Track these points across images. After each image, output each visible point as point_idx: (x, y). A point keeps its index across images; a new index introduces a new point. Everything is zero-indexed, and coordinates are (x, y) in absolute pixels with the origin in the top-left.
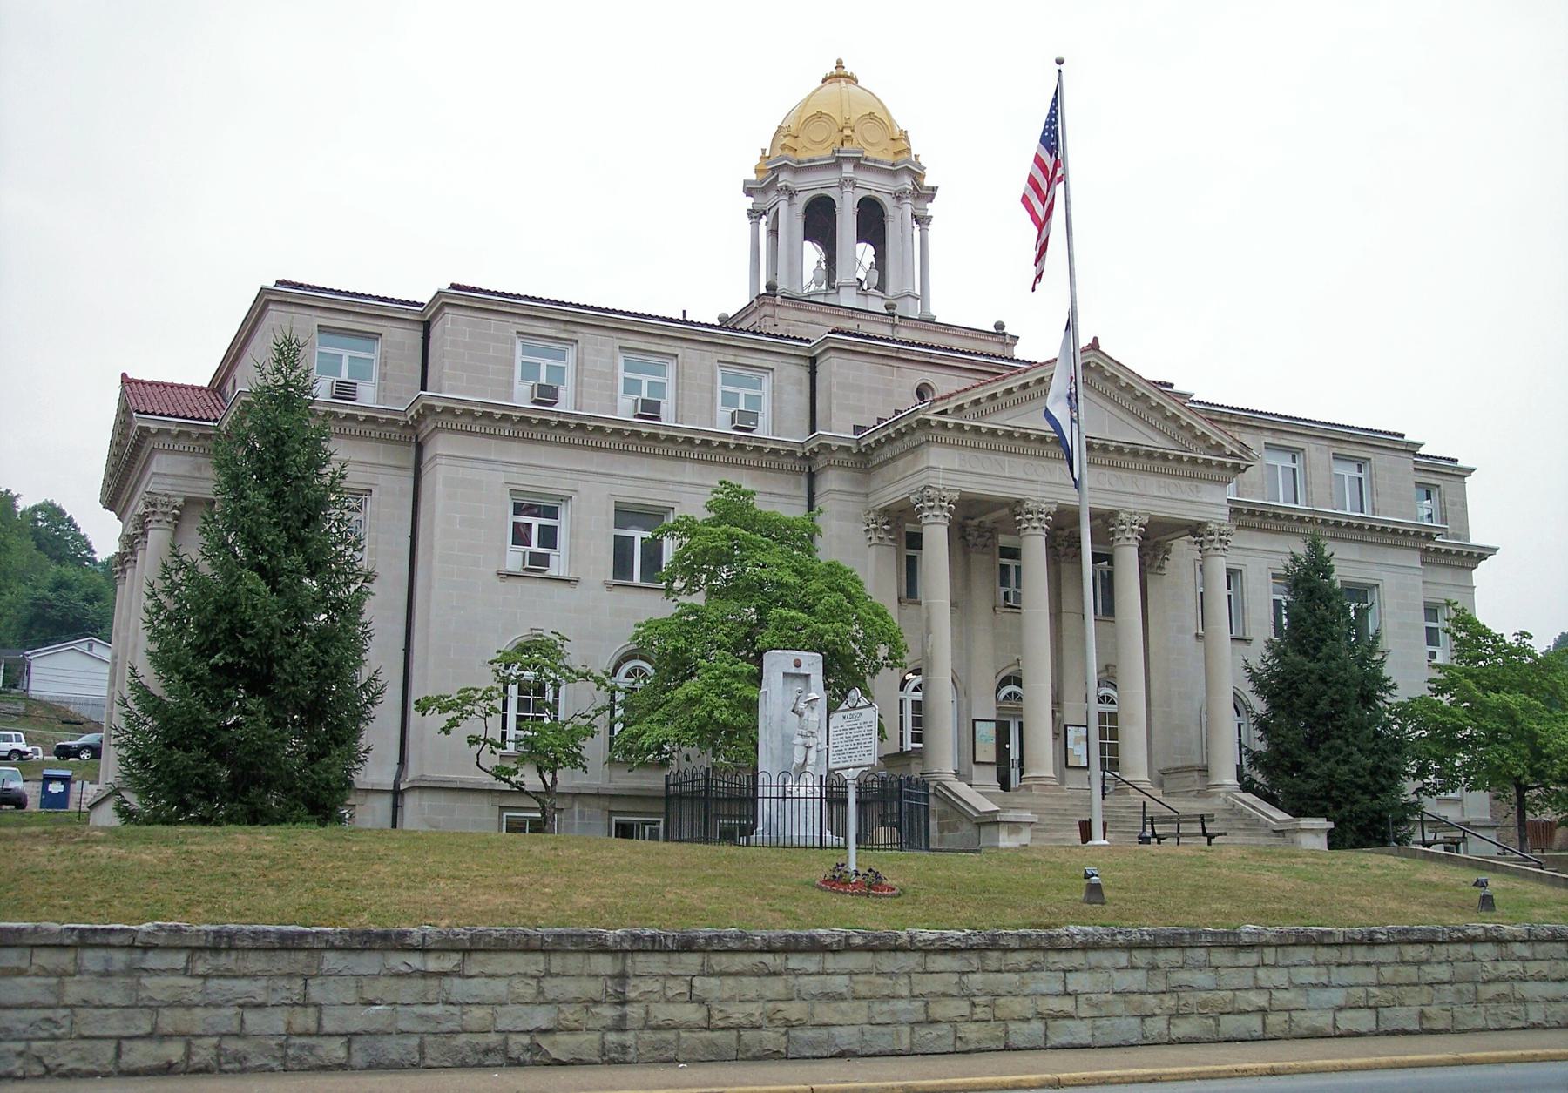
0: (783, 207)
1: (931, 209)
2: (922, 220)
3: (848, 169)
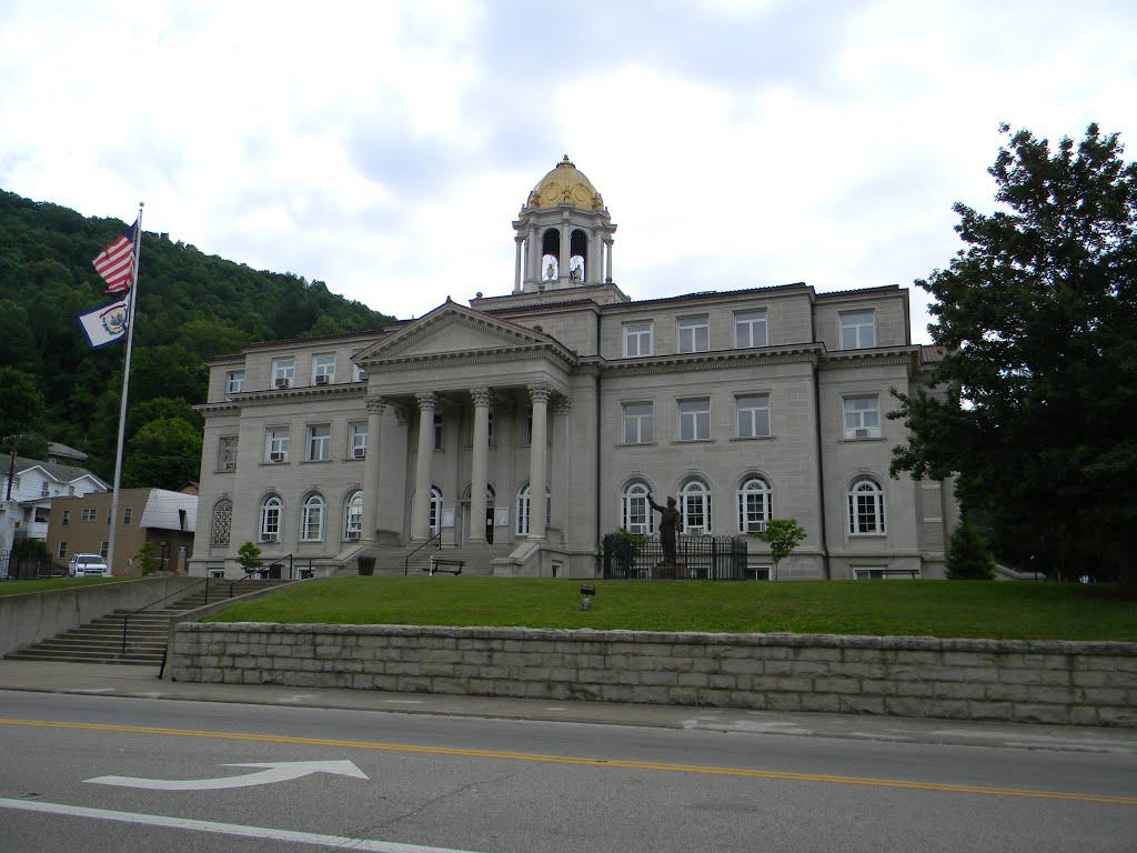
0: (532, 234)
1: (613, 236)
2: (610, 242)
3: (566, 215)
